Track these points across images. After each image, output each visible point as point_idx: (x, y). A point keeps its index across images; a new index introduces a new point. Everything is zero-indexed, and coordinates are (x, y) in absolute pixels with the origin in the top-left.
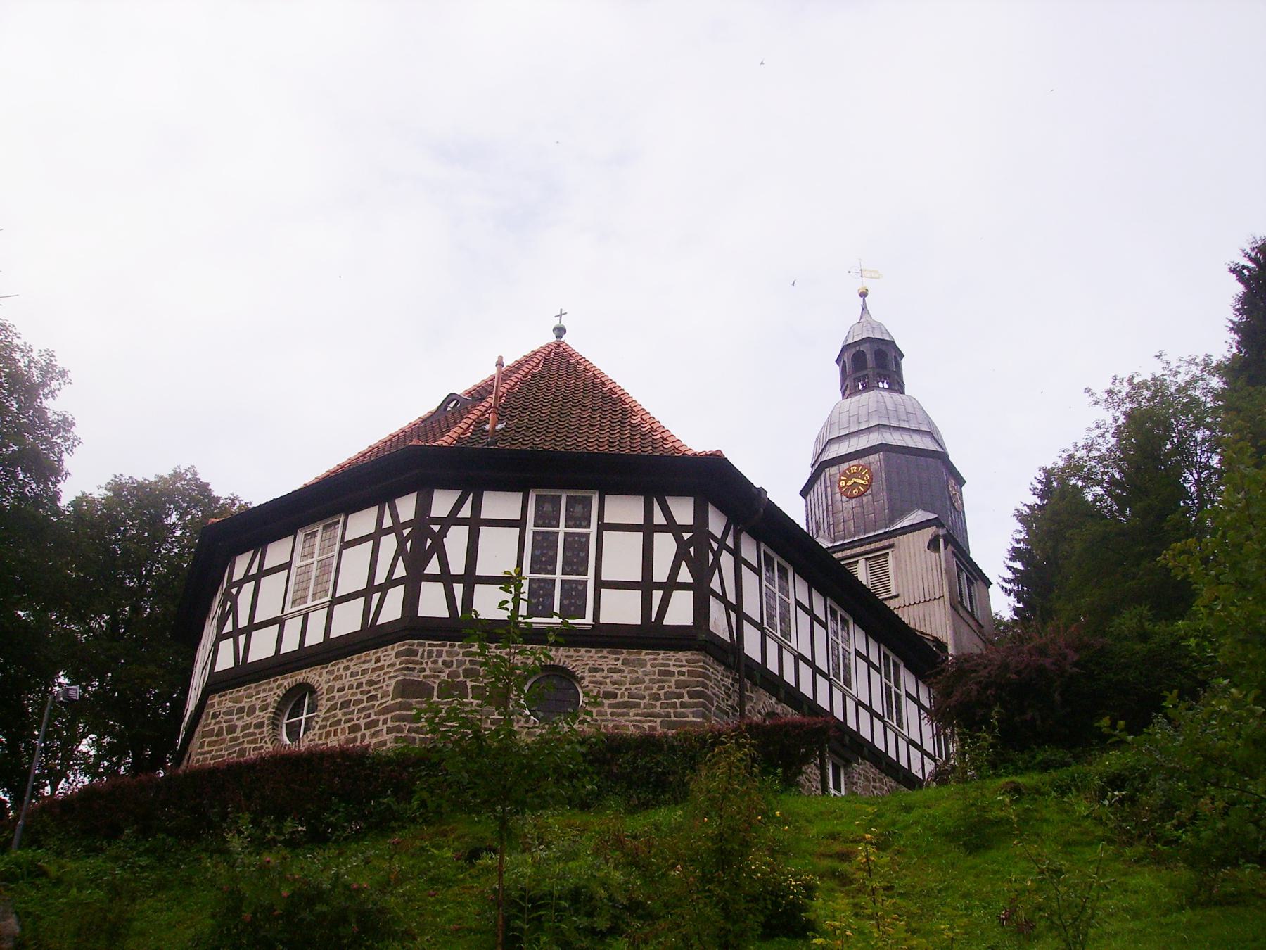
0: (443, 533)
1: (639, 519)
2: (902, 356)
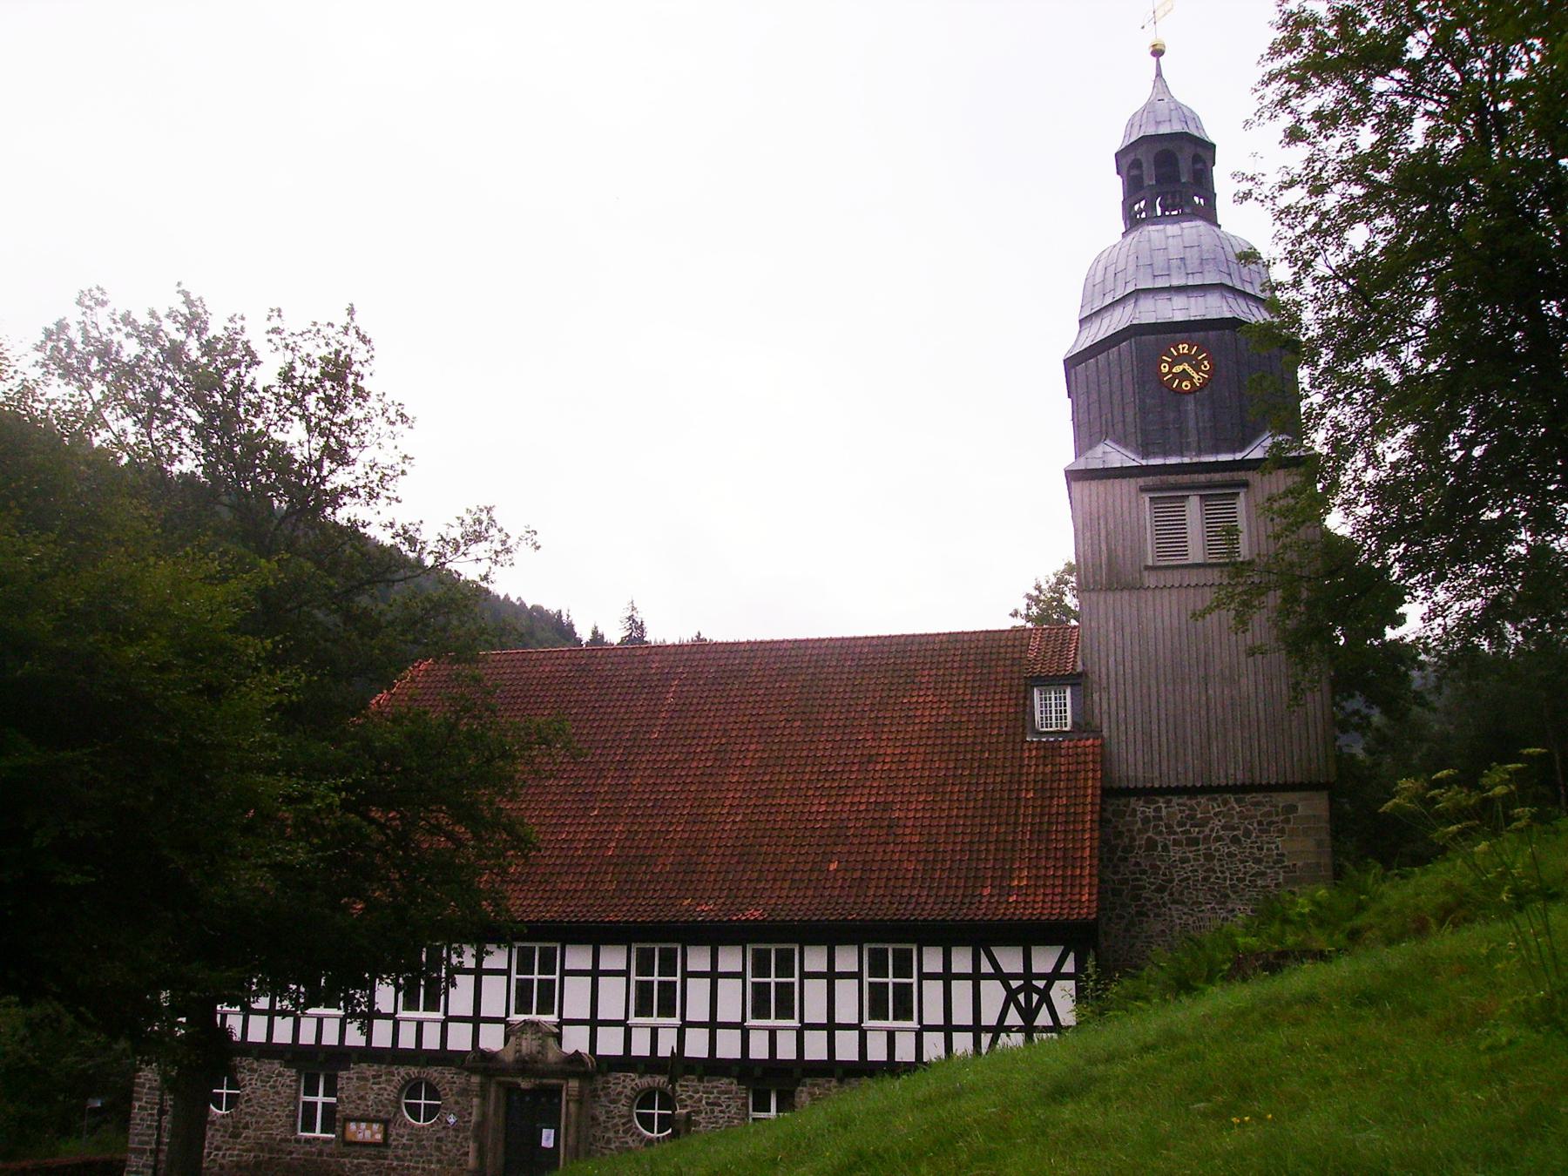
0: (1049, 986)
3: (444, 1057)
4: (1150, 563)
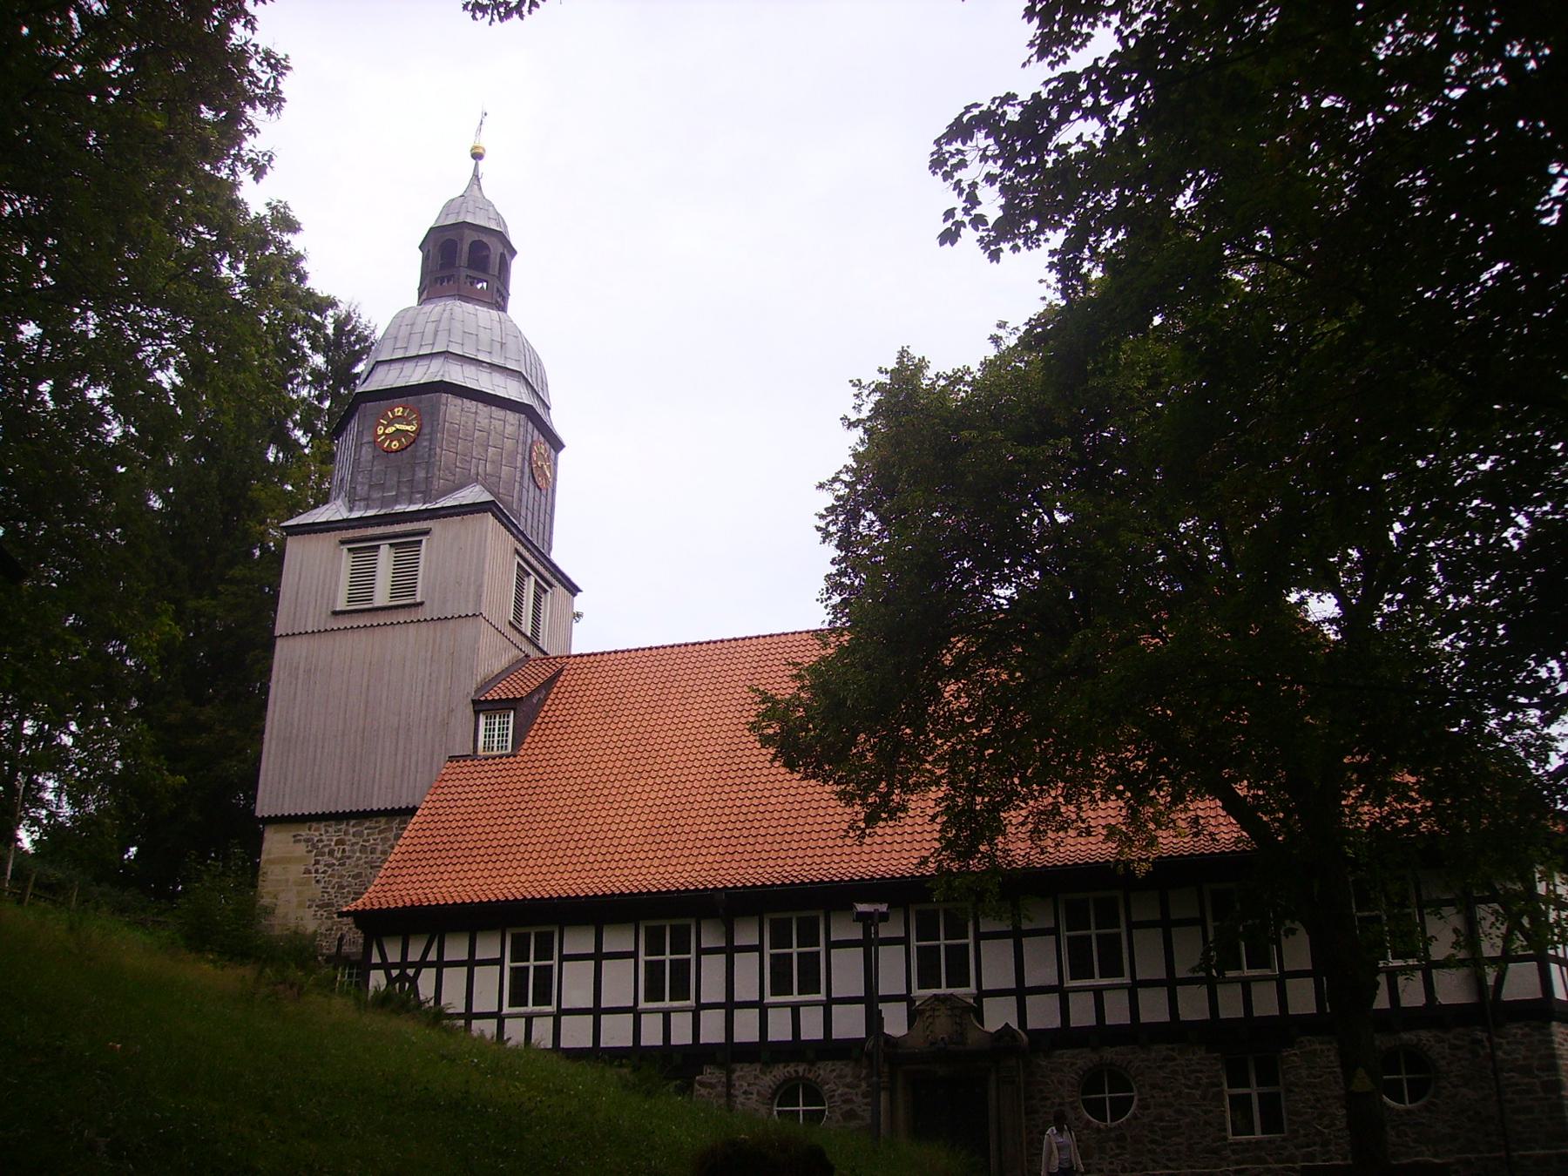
0: (417, 974)
1: (1156, 915)
2: (513, 252)
3: (830, 1049)
4: (341, 605)
